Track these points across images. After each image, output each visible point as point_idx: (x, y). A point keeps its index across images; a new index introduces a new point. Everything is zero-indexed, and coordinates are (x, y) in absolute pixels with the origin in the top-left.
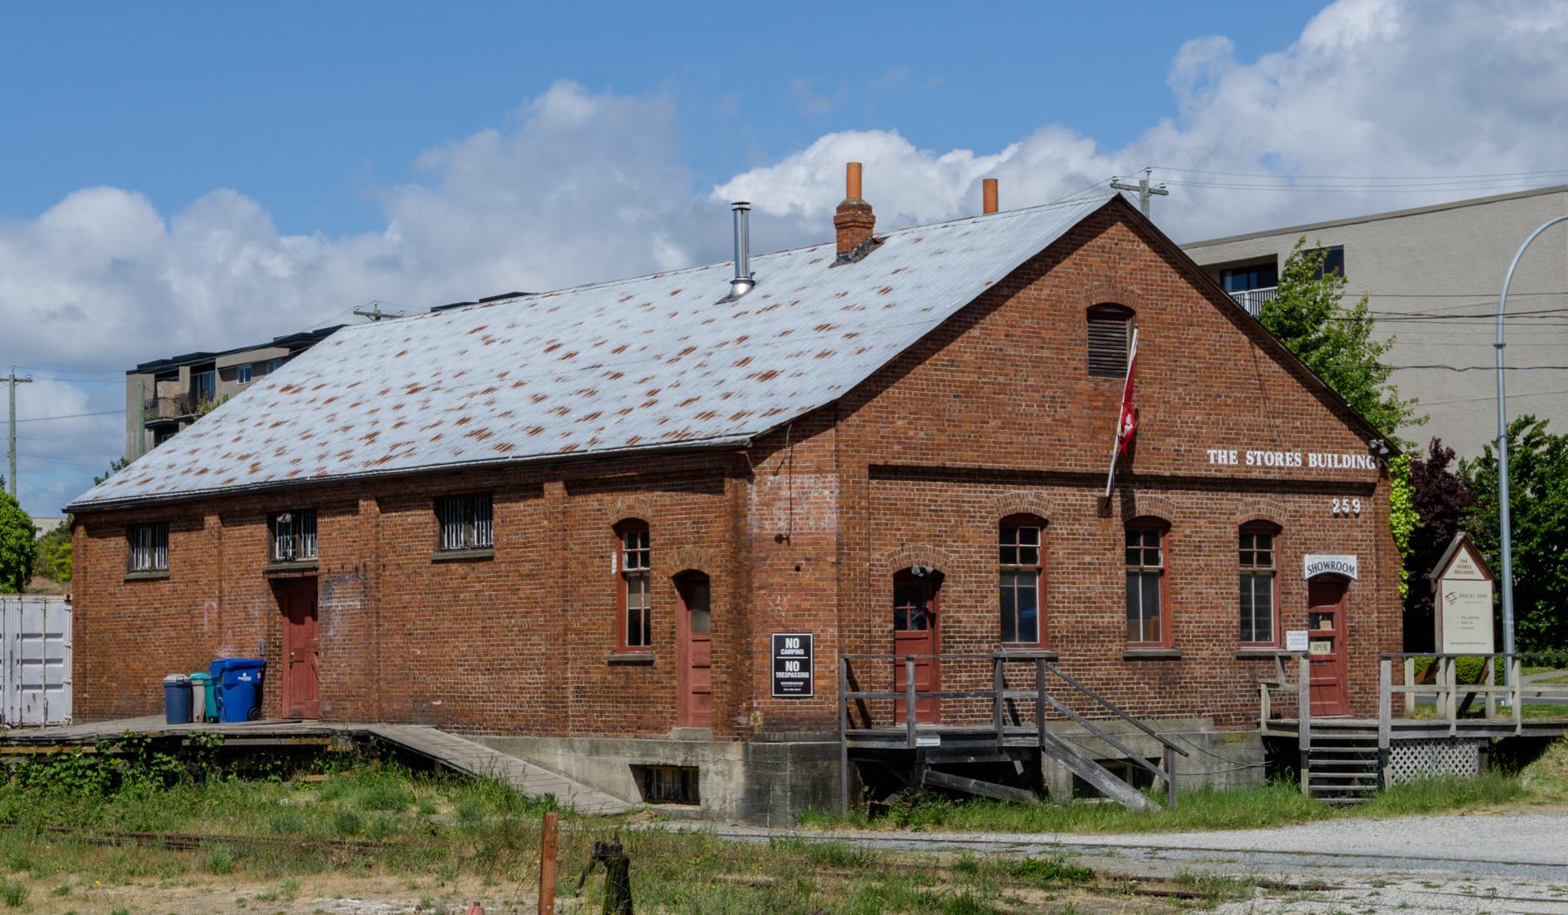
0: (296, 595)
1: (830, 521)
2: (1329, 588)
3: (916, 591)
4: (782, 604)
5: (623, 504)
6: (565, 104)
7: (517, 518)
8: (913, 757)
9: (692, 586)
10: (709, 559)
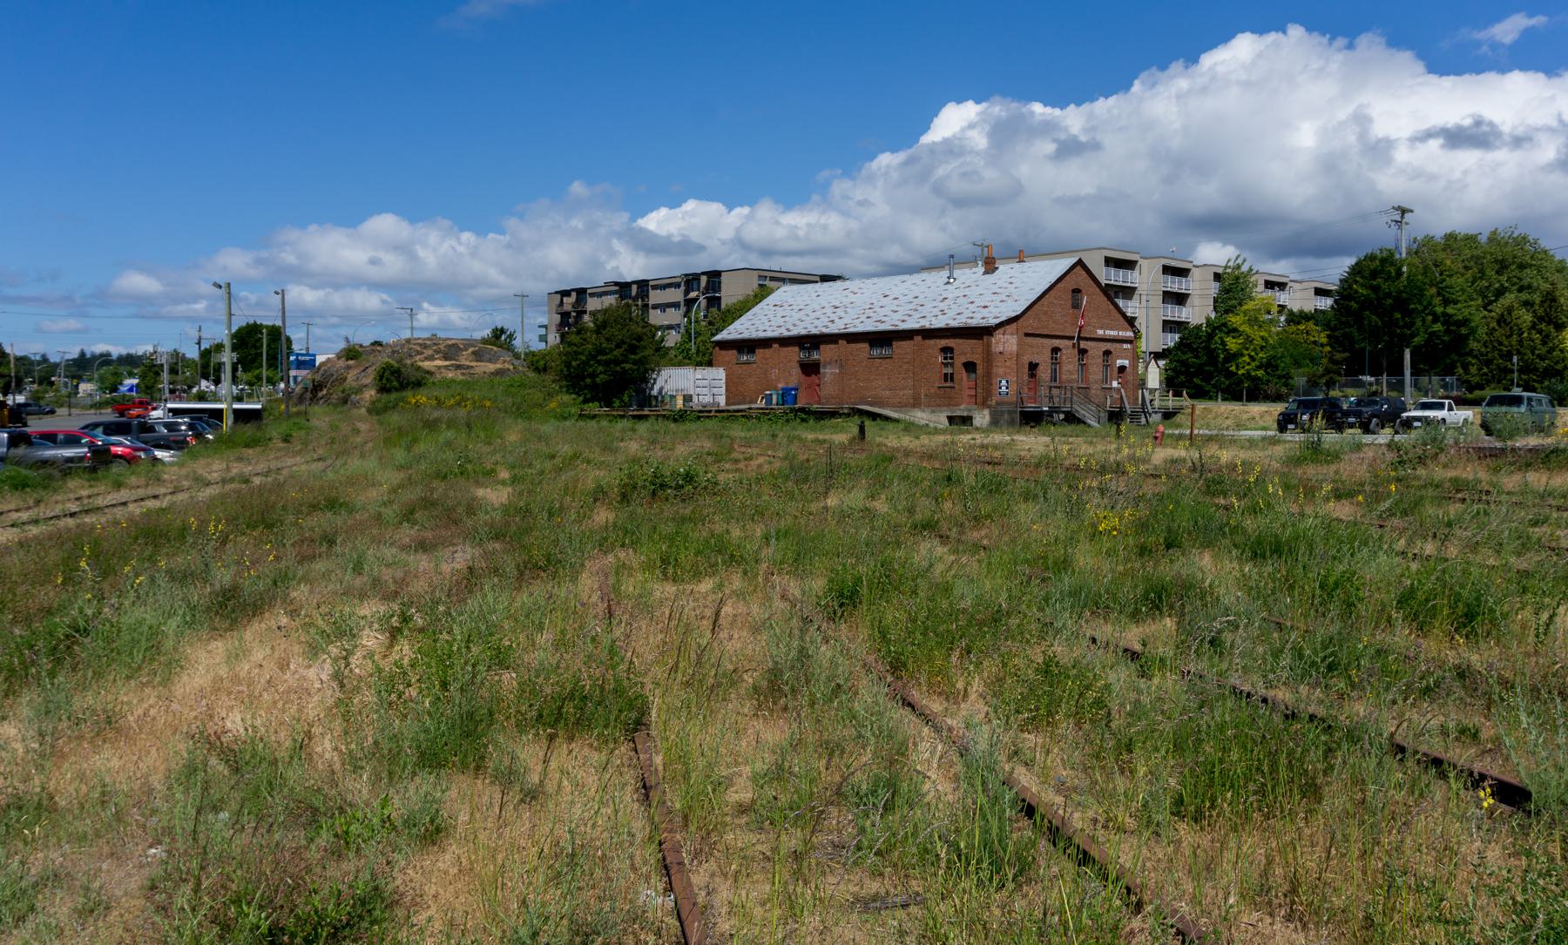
0: (810, 369)
1: (1015, 348)
2: (1122, 369)
3: (1033, 367)
4: (1001, 371)
5: (944, 343)
6: (577, 188)
7: (900, 347)
8: (1042, 412)
9: (970, 367)
10: (976, 358)
